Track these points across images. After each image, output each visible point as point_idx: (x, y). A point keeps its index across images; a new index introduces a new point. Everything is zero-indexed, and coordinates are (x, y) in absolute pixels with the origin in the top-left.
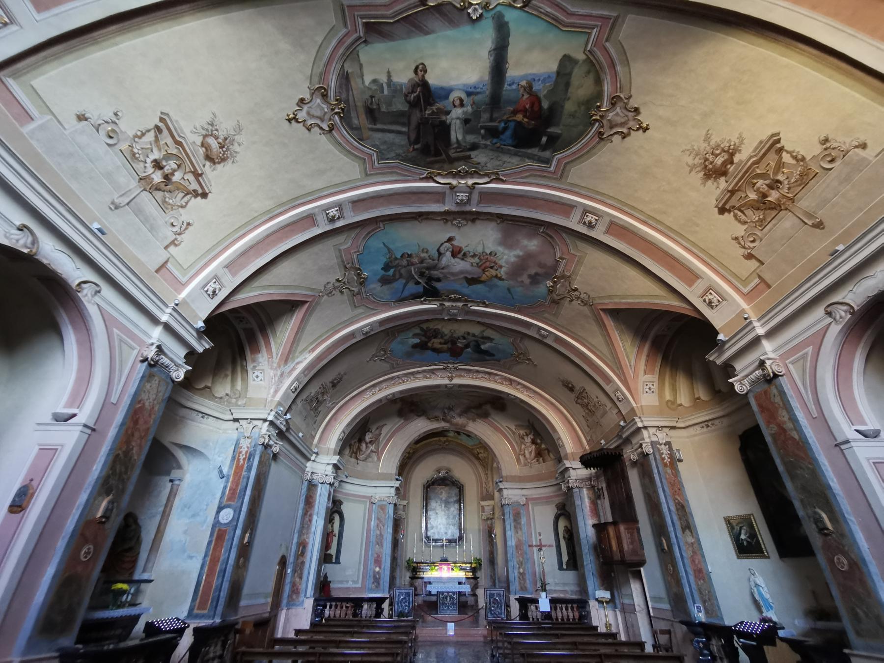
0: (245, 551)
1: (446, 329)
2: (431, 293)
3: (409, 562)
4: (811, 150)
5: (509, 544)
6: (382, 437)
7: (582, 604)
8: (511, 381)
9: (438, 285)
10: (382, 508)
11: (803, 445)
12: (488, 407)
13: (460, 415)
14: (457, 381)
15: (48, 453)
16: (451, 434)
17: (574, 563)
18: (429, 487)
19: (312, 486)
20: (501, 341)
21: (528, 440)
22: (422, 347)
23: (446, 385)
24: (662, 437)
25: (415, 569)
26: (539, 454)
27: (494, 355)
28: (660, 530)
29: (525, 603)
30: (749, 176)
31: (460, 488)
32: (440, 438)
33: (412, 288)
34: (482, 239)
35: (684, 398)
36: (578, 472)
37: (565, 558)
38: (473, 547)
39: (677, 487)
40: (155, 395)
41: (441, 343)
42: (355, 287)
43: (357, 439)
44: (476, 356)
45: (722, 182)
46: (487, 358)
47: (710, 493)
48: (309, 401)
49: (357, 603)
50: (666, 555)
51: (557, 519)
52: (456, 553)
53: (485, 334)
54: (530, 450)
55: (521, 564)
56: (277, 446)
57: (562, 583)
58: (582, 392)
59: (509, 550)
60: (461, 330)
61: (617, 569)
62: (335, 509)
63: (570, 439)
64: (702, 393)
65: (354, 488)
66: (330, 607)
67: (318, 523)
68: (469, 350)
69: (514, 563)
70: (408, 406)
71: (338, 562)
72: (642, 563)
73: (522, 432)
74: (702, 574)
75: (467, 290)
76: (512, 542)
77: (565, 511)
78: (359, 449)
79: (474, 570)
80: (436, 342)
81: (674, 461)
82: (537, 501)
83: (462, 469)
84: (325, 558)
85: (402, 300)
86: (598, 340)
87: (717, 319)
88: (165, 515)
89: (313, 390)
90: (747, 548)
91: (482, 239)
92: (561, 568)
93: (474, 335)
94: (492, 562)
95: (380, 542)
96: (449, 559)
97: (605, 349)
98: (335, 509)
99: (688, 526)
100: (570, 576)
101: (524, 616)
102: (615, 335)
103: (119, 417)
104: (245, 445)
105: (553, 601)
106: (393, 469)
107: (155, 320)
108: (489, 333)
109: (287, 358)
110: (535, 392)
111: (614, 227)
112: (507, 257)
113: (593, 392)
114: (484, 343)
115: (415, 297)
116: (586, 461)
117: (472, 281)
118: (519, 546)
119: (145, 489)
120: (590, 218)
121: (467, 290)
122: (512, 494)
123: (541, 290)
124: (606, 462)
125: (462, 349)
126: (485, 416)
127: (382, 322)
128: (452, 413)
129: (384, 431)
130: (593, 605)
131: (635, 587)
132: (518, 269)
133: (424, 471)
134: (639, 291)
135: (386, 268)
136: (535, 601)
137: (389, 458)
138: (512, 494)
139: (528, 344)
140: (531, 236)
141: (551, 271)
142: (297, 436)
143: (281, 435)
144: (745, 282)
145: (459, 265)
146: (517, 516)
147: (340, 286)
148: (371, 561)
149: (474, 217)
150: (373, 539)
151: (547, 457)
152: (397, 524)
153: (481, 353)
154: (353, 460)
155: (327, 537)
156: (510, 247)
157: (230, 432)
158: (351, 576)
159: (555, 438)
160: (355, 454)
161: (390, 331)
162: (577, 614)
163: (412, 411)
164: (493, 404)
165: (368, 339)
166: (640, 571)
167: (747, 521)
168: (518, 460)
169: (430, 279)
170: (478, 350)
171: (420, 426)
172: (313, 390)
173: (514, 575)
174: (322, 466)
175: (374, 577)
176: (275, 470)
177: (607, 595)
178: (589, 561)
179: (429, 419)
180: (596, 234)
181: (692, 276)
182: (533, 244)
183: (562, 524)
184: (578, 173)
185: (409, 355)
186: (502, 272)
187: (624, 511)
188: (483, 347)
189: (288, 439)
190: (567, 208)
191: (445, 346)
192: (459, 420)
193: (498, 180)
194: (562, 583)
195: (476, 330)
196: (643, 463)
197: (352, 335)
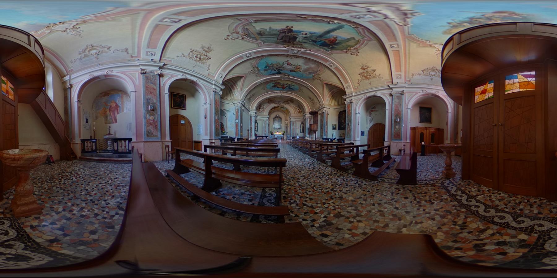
0: (241, 127)
1: (282, 82)
2: (279, 73)
4: (377, 74)
7: (304, 137)
9: (281, 71)
11: (351, 113)
15: (206, 109)
17: (303, 131)
18: (274, 118)
19: (251, 117)
20: (296, 86)
22: (275, 86)
24: (327, 110)
25: (272, 133)
26: (299, 112)
28: (322, 125)
29: (293, 137)
30: (368, 72)
31: (281, 119)
32: (277, 107)
33: (273, 72)
34: (299, 62)
35: (333, 104)
36: (308, 115)
38: (284, 129)
39: (327, 118)
40: (218, 98)
42: (257, 71)
43: (259, 108)
45: (363, 71)
47: (332, 119)
48: (248, 99)
49: (263, 137)
50: (322, 129)
56: (243, 108)
57: (302, 135)
58: (313, 99)
60: (285, 83)
61: (312, 131)
62: (256, 122)
63: (307, 109)
64: (336, 104)
65: (259, 118)
67: (253, 124)
70: (270, 100)
74: (327, 132)
75: (290, 73)
76: (292, 128)
77: (303, 123)
80: (278, 85)
81: (328, 114)
82: (297, 121)
83: (281, 115)
84: (256, 131)
85: (270, 75)
86: (321, 89)
87: (347, 91)
88: (226, 122)
89: (249, 96)
90: (334, 129)
91: (299, 62)
95: (265, 128)
97: (321, 92)
98: (256, 122)
99: (327, 125)
100: (302, 134)
102: (325, 89)
103: (213, 102)
104: (237, 108)
106: (267, 114)
107: (212, 84)
108: (293, 84)
109: (241, 90)
111: (337, 68)
112: (304, 67)
113: (315, 99)
115: (274, 74)
116: (310, 113)
117: (291, 71)
118: (293, 129)
119: (222, 118)
120: (332, 64)
121: (290, 73)
122: (293, 119)
123: (311, 76)
124: (314, 114)
126: (289, 103)
127: (264, 80)
131: (314, 135)
132: (306, 70)
133: (273, 115)
134: (335, 81)
135: (266, 67)
137: (266, 112)
138: (293, 119)
139: (303, 87)
140: (313, 64)
141: (316, 73)
142: (247, 106)
143: (243, 106)
145: (289, 67)
146: (293, 124)
147: (252, 72)
149: (297, 57)
152: (268, 125)
153: (290, 89)
155: (255, 126)
156: (306, 65)
157: (233, 106)
158: (260, 133)
160: (259, 111)
161: (266, 82)
164: (291, 100)
165: (261, 84)
167: (336, 125)
169: (279, 70)
170: (290, 88)
171: (273, 105)
172: (249, 96)
173: (292, 134)
174: (253, 113)
176: (243, 113)
178: (307, 131)
180: (332, 68)
181: (347, 82)
182: (313, 66)
184: (334, 56)
185: (271, 88)
186: (301, 70)
187: (316, 122)
188: (456, 203)
189: (244, 107)
190: (327, 61)
193: (310, 50)
195: (290, 83)
196: (322, 115)
197: (257, 83)
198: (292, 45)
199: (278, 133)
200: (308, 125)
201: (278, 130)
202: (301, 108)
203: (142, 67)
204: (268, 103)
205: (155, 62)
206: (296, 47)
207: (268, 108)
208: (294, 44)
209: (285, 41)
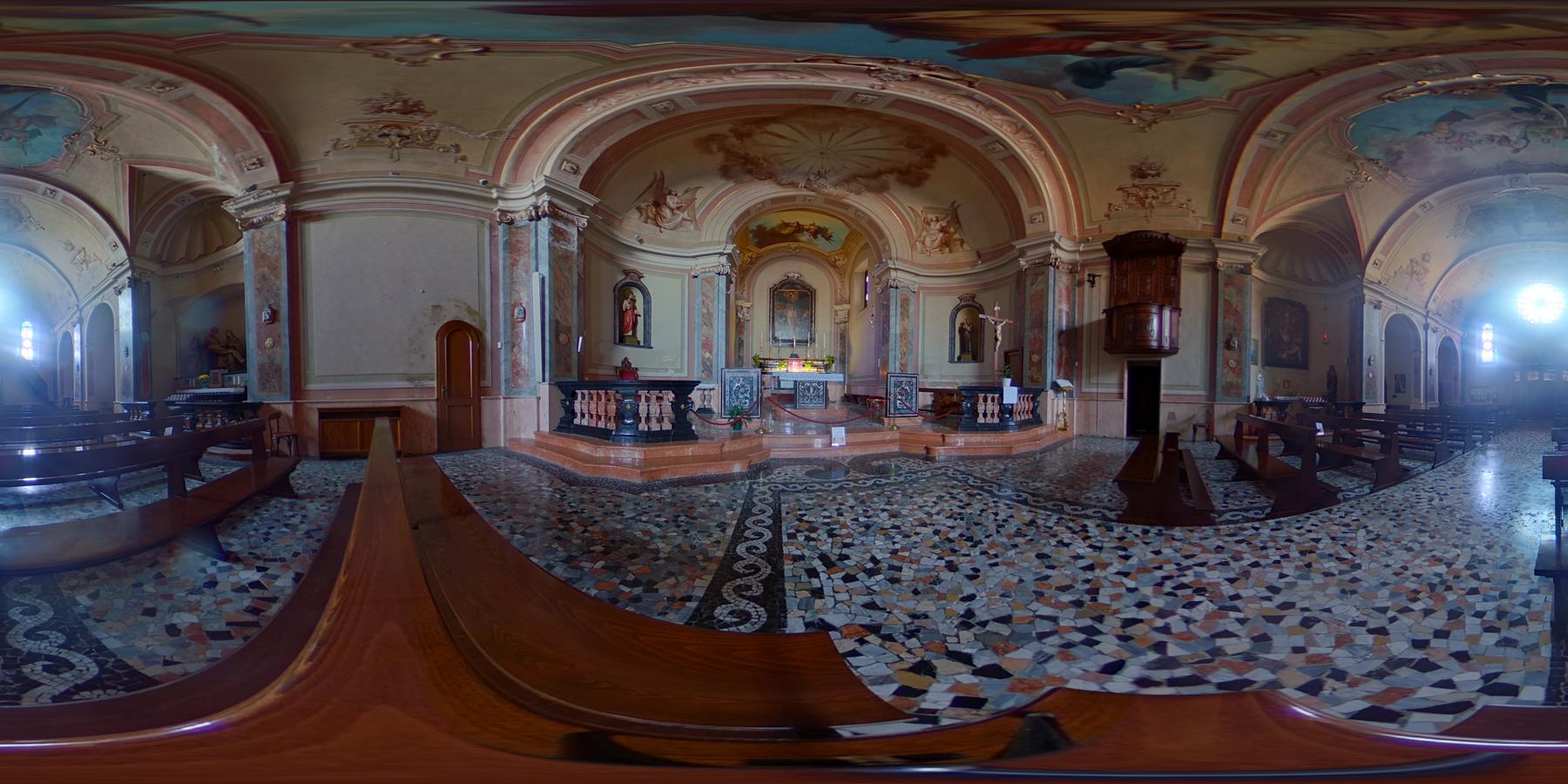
5: (892, 331)
6: (697, 203)
10: (708, 281)
12: (891, 178)
13: (835, 185)
16: (805, 237)
26: (946, 244)
37: (957, 354)
51: (958, 309)
54: (934, 236)
59: (892, 338)
66: (648, 399)
71: (647, 345)
76: (895, 328)
78: (658, 213)
92: (951, 361)
95: (708, 320)
96: (802, 356)
118: (904, 335)
126: (880, 190)
128: (822, 181)
129: (700, 196)
150: (698, 320)
154: (650, 227)
163: (749, 172)
168: (913, 247)
175: (704, 364)
179: (780, 184)
183: (961, 318)
192: (835, 191)
199: (795, 368)
201: (799, 351)
202: (988, 209)
204: (725, 172)
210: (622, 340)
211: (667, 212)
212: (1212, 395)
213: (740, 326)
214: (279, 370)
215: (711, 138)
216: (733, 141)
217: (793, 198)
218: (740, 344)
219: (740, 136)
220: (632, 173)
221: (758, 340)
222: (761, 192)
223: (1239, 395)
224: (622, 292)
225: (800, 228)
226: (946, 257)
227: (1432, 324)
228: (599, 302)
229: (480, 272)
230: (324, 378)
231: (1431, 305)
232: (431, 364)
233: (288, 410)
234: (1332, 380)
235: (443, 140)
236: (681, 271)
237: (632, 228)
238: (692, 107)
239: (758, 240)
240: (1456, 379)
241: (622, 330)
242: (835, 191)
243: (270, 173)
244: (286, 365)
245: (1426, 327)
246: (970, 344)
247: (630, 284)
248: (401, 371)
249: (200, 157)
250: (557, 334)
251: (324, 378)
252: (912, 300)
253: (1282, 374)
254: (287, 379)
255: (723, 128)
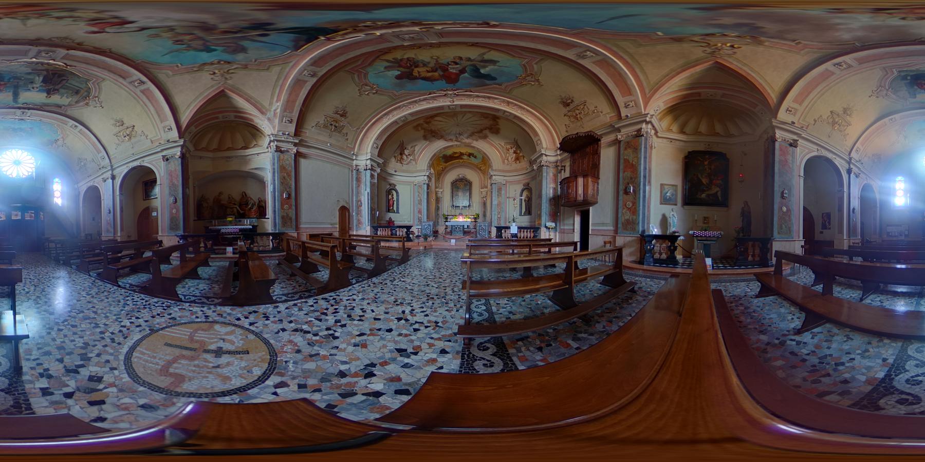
1: (424, 56)
3: (444, 215)
7: (536, 229)
8: (508, 103)
10: (420, 186)
12: (487, 132)
13: (467, 138)
14: (458, 102)
16: (465, 157)
21: (512, 151)
23: (449, 106)
26: (517, 159)
27: (494, 79)
29: (499, 229)
38: (477, 208)
41: (428, 72)
44: (476, 81)
46: (488, 82)
51: (523, 191)
52: (465, 212)
53: (486, 57)
55: (499, 213)
57: (525, 221)
68: (466, 75)
69: (495, 212)
71: (398, 212)
72: (593, 203)
73: (508, 147)
76: (495, 202)
78: (402, 158)
79: (475, 218)
82: (511, 183)
92: (521, 215)
93: (469, 59)
94: (485, 215)
95: (420, 202)
101: (499, 235)
105: (520, 228)
110: (528, 111)
114: (484, 67)
118: (499, 204)
125: (457, 76)
129: (417, 148)
130: (543, 229)
136: (508, 228)
144: (804, 120)
146: (500, 190)
148: (416, 211)
150: (417, 202)
151: (522, 159)
153: (481, 78)
154: (399, 164)
159: (535, 139)
162: (532, 235)
166: (588, 211)
168: (504, 162)
170: (476, 73)
177: (553, 225)
178: (545, 207)
183: (525, 194)
188: (482, 71)
191: (436, 74)
192: (467, 141)
194: (525, 221)
195: (473, 54)
198: (51, 68)
200: (549, 188)
202: (523, 144)
203: (164, 153)
204: (425, 138)
205: (175, 142)
206: (42, 64)
207: (425, 153)
208: (47, 70)
209: (60, 76)
210: (389, 211)
211: (405, 157)
212: (616, 231)
213: (438, 200)
214: (291, 219)
215: (418, 125)
216: (426, 125)
217: (452, 146)
218: (438, 209)
219: (427, 123)
220: (394, 145)
221: (446, 207)
222: (439, 145)
223: (634, 229)
224: (389, 192)
225: (462, 154)
226: (518, 166)
227: (854, 169)
228: (384, 195)
229: (316, 223)
230: (306, 223)
231: (853, 154)
232: (337, 220)
233: (295, 235)
234: (746, 215)
235: (344, 131)
236: (411, 179)
237: (393, 166)
238: (410, 118)
239: (445, 161)
240: (875, 206)
241: (389, 207)
242: (467, 141)
243: (292, 128)
244: (294, 217)
245: (849, 172)
246: (529, 208)
247: (392, 189)
248: (329, 223)
249: (266, 104)
250: (372, 210)
251: (306, 223)
252: (503, 188)
253: (700, 212)
254: (294, 223)
255: (421, 122)
